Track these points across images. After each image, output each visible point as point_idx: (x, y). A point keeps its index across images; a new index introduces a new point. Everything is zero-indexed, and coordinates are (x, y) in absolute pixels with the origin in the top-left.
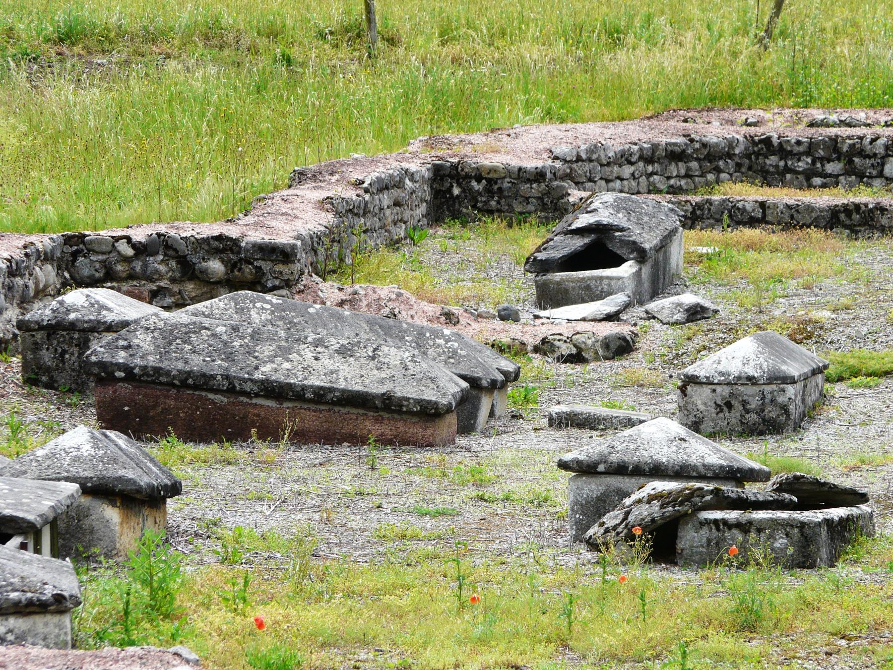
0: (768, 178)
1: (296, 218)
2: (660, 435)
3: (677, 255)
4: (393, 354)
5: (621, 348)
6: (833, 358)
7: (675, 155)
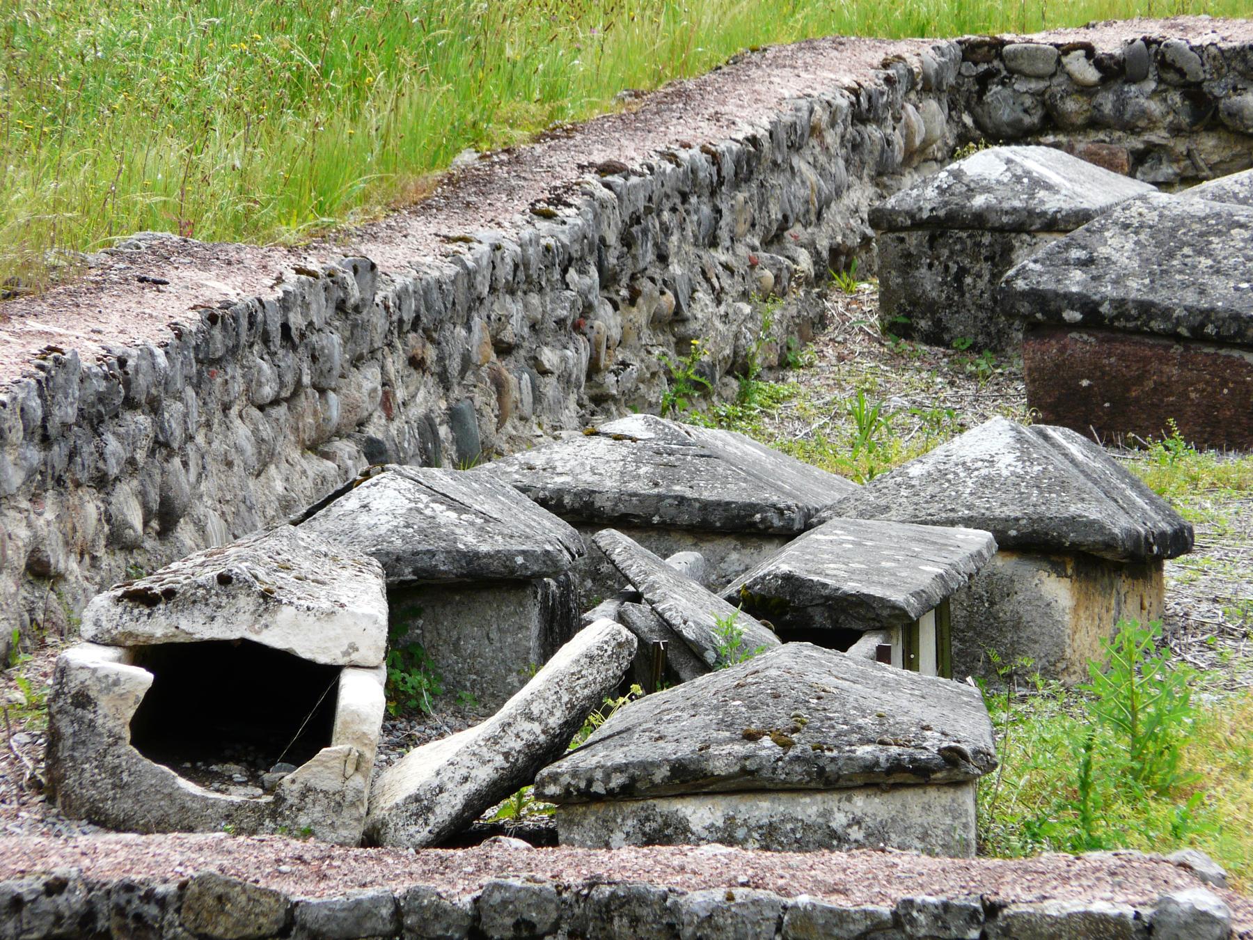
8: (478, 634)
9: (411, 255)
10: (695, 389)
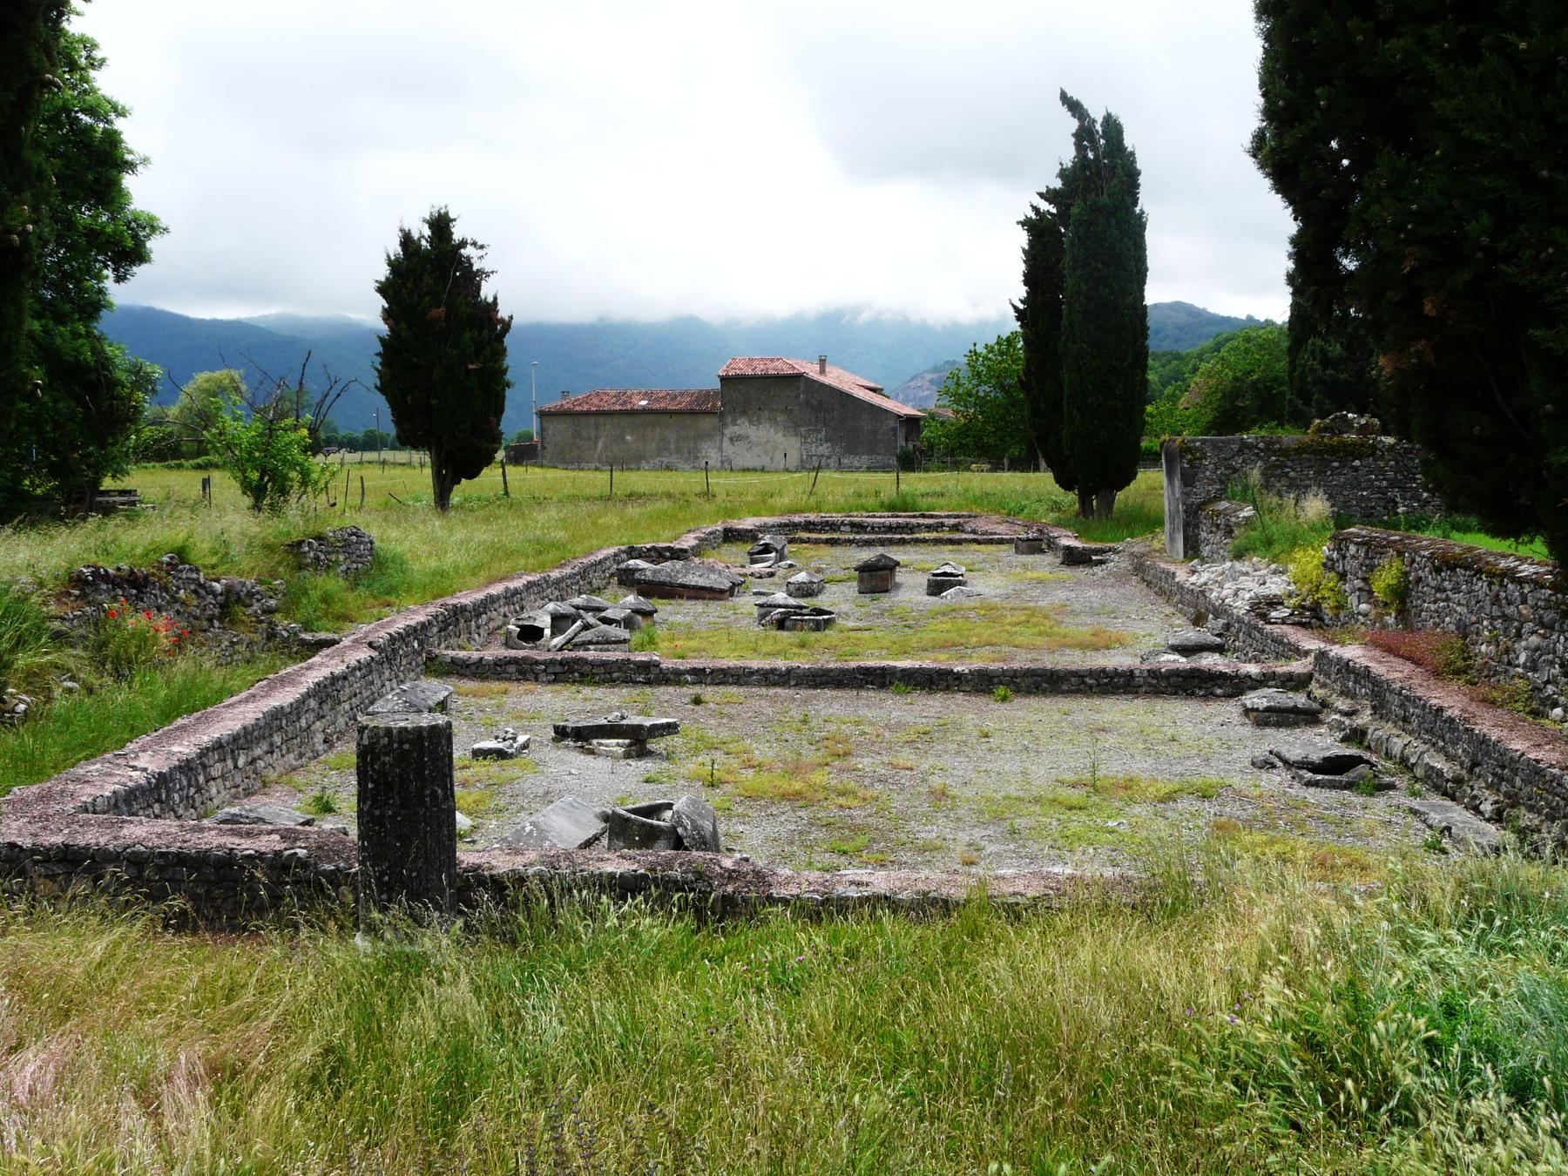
0: (810, 531)
1: (688, 542)
2: (780, 597)
3: (786, 551)
4: (713, 576)
5: (772, 575)
6: (828, 576)
7: (786, 525)
8: (563, 624)
9: (555, 574)
10: (592, 592)
